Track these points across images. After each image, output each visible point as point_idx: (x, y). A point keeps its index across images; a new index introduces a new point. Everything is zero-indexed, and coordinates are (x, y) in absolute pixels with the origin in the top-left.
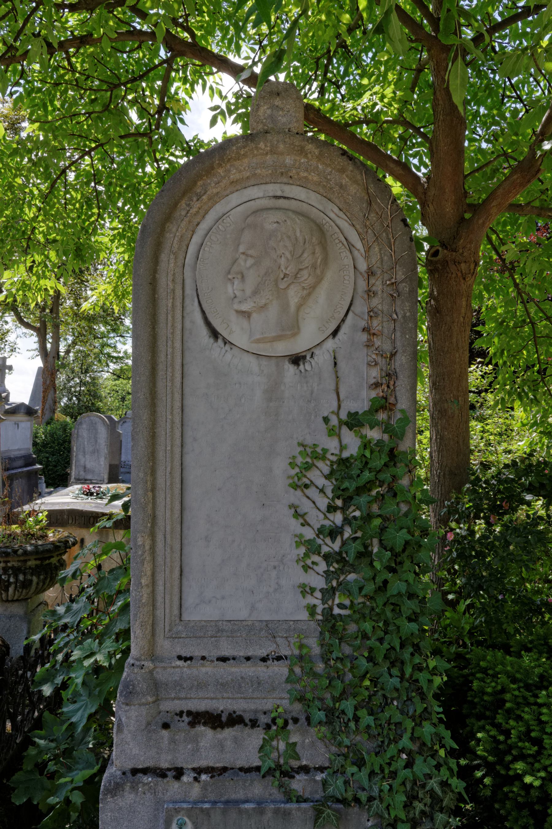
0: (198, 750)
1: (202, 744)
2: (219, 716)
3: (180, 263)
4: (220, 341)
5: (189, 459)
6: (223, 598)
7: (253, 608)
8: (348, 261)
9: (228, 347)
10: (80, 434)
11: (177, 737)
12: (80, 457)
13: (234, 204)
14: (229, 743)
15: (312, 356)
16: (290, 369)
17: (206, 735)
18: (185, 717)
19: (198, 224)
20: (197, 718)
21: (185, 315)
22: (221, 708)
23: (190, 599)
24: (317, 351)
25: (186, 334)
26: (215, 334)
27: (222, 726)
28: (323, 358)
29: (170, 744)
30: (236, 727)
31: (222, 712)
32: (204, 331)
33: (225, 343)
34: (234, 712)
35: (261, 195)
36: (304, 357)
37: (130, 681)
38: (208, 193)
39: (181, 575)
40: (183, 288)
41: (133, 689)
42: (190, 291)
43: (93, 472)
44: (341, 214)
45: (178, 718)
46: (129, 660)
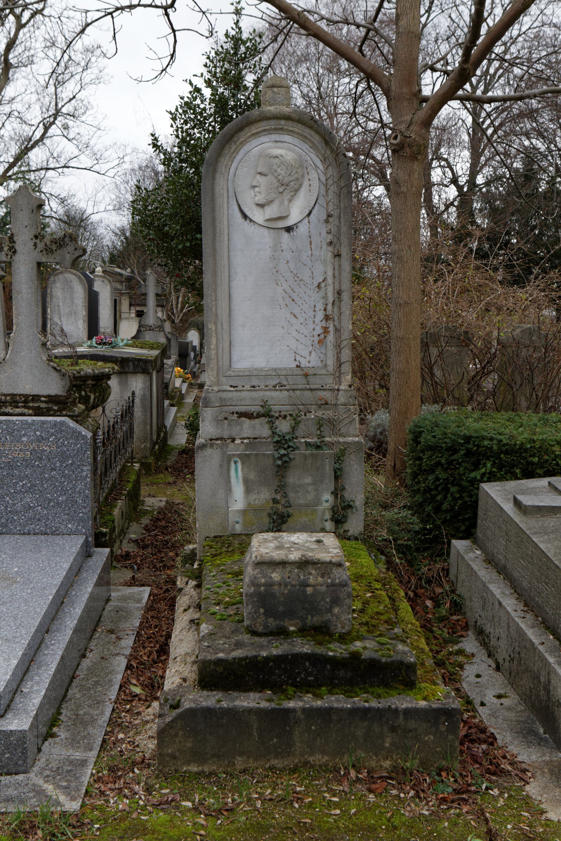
2: (252, 414)
5: (233, 284)
7: (268, 362)
8: (315, 175)
10: (54, 293)
13: (254, 145)
16: (285, 235)
20: (241, 415)
23: (235, 357)
24: (299, 225)
26: (245, 216)
27: (255, 418)
28: (303, 229)
32: (239, 215)
42: (231, 193)
44: (311, 150)
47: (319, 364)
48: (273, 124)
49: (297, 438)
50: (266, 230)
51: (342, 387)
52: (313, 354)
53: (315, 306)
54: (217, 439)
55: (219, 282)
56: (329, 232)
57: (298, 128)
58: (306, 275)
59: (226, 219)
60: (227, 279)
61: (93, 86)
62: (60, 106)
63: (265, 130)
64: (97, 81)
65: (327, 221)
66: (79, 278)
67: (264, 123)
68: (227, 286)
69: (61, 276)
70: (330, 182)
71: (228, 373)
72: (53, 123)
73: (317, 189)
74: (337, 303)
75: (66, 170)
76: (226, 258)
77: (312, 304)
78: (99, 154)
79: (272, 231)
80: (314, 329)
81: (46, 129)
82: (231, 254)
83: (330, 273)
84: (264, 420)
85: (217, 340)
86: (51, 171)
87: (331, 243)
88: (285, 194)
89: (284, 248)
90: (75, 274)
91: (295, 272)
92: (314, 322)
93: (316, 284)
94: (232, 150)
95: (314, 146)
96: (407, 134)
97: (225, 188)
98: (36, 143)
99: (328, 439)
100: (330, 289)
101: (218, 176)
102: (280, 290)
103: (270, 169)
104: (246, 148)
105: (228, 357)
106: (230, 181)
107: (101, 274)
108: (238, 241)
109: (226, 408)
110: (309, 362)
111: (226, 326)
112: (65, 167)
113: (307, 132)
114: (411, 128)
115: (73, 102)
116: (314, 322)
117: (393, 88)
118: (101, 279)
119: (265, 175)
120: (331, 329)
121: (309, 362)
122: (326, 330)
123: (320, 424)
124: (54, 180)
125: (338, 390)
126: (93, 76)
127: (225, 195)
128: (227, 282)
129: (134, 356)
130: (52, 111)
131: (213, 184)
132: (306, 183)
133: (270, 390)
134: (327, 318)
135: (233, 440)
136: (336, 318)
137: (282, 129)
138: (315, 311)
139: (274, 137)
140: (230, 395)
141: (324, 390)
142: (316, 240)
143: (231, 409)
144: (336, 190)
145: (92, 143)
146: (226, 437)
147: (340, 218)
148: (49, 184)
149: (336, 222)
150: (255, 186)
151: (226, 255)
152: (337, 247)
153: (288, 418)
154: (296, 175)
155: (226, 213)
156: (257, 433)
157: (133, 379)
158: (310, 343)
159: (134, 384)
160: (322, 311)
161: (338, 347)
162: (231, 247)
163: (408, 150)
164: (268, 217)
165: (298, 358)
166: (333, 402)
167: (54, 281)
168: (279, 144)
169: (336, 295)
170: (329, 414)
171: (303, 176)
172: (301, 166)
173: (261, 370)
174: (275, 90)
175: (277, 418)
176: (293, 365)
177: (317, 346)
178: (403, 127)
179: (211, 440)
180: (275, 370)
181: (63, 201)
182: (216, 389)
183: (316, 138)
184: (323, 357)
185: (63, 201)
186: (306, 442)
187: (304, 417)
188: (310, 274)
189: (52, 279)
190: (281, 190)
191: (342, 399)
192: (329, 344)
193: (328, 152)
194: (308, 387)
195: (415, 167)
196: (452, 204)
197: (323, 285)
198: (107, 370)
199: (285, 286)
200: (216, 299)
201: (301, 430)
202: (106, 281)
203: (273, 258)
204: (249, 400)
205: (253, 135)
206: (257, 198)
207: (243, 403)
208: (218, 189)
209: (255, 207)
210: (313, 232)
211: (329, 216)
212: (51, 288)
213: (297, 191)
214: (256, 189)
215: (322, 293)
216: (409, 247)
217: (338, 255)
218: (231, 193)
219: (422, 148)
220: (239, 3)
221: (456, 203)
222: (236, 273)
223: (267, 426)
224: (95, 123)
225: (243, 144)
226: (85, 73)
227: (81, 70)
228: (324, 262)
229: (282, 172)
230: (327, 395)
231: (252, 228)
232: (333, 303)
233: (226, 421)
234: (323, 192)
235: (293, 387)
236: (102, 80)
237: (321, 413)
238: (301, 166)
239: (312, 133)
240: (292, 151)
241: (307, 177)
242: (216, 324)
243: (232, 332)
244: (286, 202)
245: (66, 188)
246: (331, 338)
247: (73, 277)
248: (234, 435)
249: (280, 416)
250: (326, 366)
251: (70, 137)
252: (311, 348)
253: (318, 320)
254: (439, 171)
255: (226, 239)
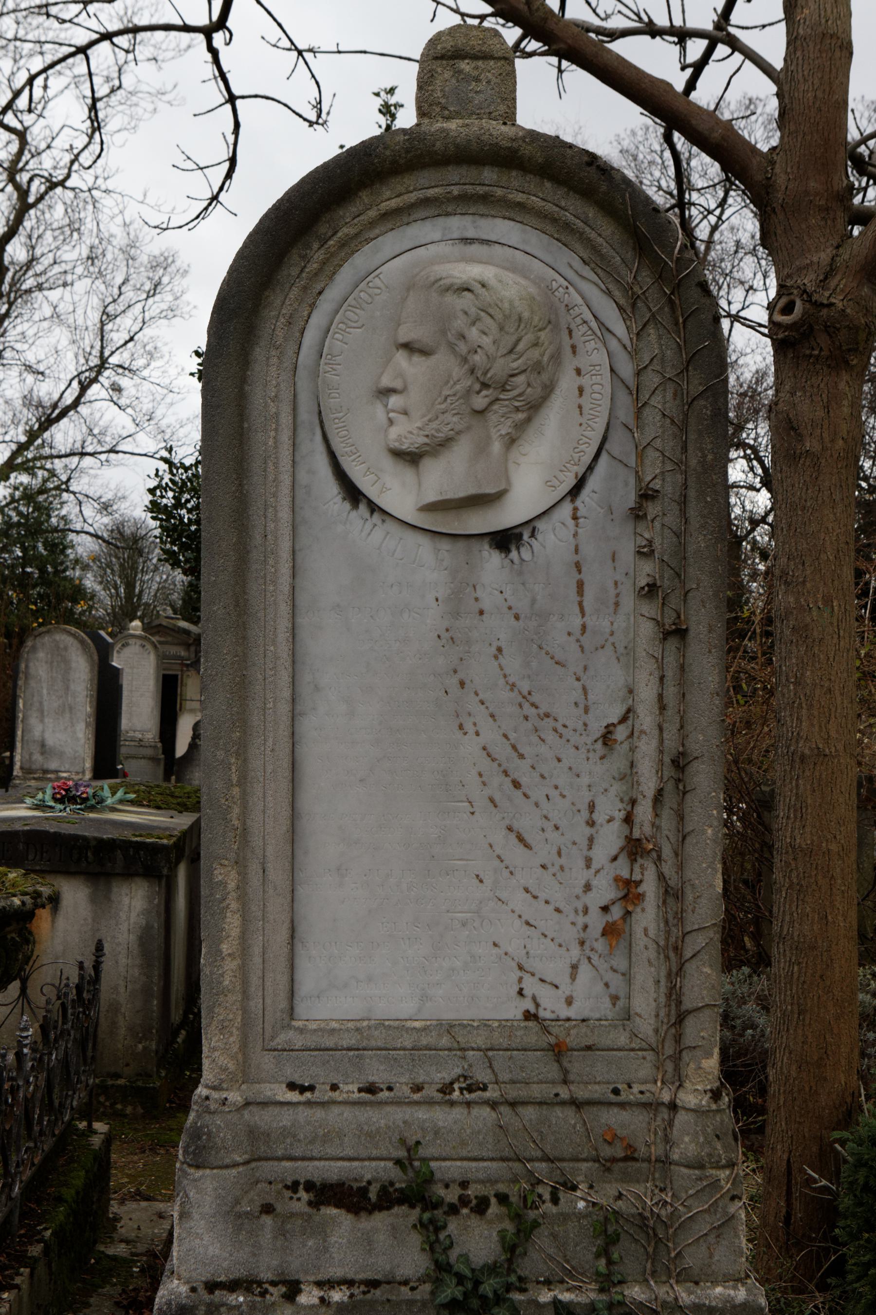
0: (326, 1250)
1: (333, 1239)
2: (363, 1192)
3: (287, 364)
4: (363, 507)
5: (308, 726)
6: (370, 979)
8: (600, 357)
9: (376, 516)
10: (32, 671)
11: (289, 1226)
12: (33, 721)
13: (388, 252)
14: (382, 1237)
15: (533, 535)
16: (493, 559)
17: (341, 1224)
18: (303, 1195)
19: (320, 293)
21: (297, 459)
22: (368, 1177)
23: (307, 982)
24: (541, 525)
25: (300, 494)
26: (353, 494)
27: (373, 1208)
28: (553, 542)
29: (275, 1238)
30: (396, 1210)
31: (369, 1183)
32: (331, 488)
33: (372, 512)
34: (392, 1184)
35: (437, 236)
36: (520, 536)
37: (202, 1127)
38: (340, 234)
39: (292, 937)
40: (295, 409)
41: (209, 1139)
42: (306, 414)
43: (61, 755)
44: (587, 271)
45: (288, 1194)
46: (199, 1089)
47: (605, 1008)
48: (456, 179)
49: (522, 1286)
50: (424, 543)
51: (689, 1098)
52: (585, 971)
53: (592, 807)
54: (233, 1286)
55: (255, 719)
56: (645, 553)
57: (541, 195)
58: (563, 702)
59: (285, 500)
60: (284, 708)
61: (164, 322)
62: (107, 354)
63: (426, 202)
64: (170, 314)
65: (637, 514)
66: (82, 642)
67: (424, 177)
68: (284, 732)
69: (47, 639)
70: (652, 379)
71: (281, 1039)
72: (95, 380)
73: (606, 403)
74: (670, 800)
75: (112, 456)
76: (283, 635)
77: (581, 802)
78: (169, 431)
79: (445, 545)
80: (588, 887)
81: (84, 388)
82: (303, 620)
83: (647, 693)
84: (405, 1216)
85: (245, 920)
86: (88, 458)
87: (651, 591)
88: (493, 418)
89: (486, 604)
90: (74, 635)
91: (525, 686)
92: (588, 863)
93: (597, 728)
94: (314, 266)
95: (596, 260)
96: (823, 297)
97: (286, 395)
98: (63, 414)
99: (636, 1292)
100: (647, 747)
101: (259, 353)
102: (470, 747)
103: (444, 332)
104: (361, 261)
105: (283, 980)
106: (302, 372)
107: (139, 632)
108: (326, 576)
109: (268, 1169)
110: (569, 1001)
111: (277, 875)
112: (112, 451)
113: (573, 209)
114: (833, 283)
115: (130, 345)
116: (588, 863)
117: (781, 180)
118: (139, 642)
119: (425, 352)
120: (650, 887)
121: (569, 1001)
122: (629, 891)
123: (608, 1231)
124: (92, 472)
125: (673, 1107)
126: (164, 306)
127: (286, 419)
128: (285, 720)
129: (127, 835)
130: (94, 361)
131: (243, 380)
132: (567, 383)
133: (430, 1103)
134: (634, 848)
135: (293, 1289)
136: (667, 851)
137: (485, 199)
138: (591, 823)
139: (460, 224)
140: (286, 1118)
141: (622, 1105)
142: (598, 578)
143: (288, 1170)
144: (672, 408)
145: (158, 414)
146: (266, 1275)
147: (683, 502)
148: (85, 480)
149: (672, 519)
150: (391, 391)
151: (284, 624)
152: (674, 601)
153: (494, 1209)
154: (535, 354)
155: (286, 479)
156: (379, 1265)
157: (125, 890)
158: (571, 934)
159: (126, 900)
160: (617, 825)
161: (674, 954)
162: (303, 599)
163: (823, 340)
164: (432, 497)
165: (530, 986)
166: (657, 1151)
167: (34, 649)
168: (475, 248)
169: (669, 772)
170: (638, 1195)
171: (557, 358)
172: (551, 323)
173: (400, 1027)
174: (465, 66)
175: (453, 1210)
176: (514, 1010)
177: (601, 945)
178: (809, 280)
179: (212, 1286)
180: (450, 1028)
181: (106, 508)
182: (235, 1097)
183: (605, 232)
184: (616, 981)
185: (106, 508)
186: (556, 1302)
187: (548, 1207)
188: (577, 695)
189: (29, 643)
190: (480, 401)
191: (687, 1146)
192: (640, 940)
193: (646, 278)
194: (564, 1094)
195: (842, 385)
196: (763, 520)
197: (621, 733)
198: (17, 901)
199: (490, 735)
200: (243, 780)
201: (535, 1261)
202: (148, 646)
203: (449, 638)
204: (351, 1140)
205: (385, 216)
206: (394, 432)
207: (331, 1151)
208: (258, 397)
209: (388, 463)
210: (588, 550)
211: (646, 495)
212: (27, 661)
213: (534, 407)
214: (394, 401)
215: (617, 762)
216: (828, 601)
217: (675, 633)
218: (306, 414)
219: (862, 336)
220: (391, 91)
221: (770, 519)
222: (317, 688)
223: (415, 1239)
224: (165, 381)
225: (350, 246)
226: (151, 300)
227: (144, 296)
228: (627, 656)
229: (486, 341)
230: (632, 1124)
231: (378, 534)
232: (658, 798)
233: (267, 1220)
234: (625, 414)
235: (513, 1093)
236: (177, 313)
237: (612, 1189)
238: (551, 323)
239: (591, 212)
240: (523, 272)
241: (569, 363)
242: (240, 864)
243: (302, 891)
244: (497, 447)
245: (112, 486)
246: (647, 918)
247: (69, 640)
248: (295, 1267)
249: (464, 1201)
250: (628, 1016)
251: (123, 402)
252: (576, 952)
253: (601, 854)
254: (743, 463)
255: (285, 569)
